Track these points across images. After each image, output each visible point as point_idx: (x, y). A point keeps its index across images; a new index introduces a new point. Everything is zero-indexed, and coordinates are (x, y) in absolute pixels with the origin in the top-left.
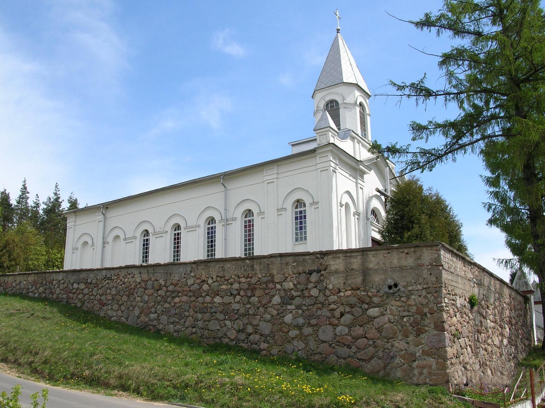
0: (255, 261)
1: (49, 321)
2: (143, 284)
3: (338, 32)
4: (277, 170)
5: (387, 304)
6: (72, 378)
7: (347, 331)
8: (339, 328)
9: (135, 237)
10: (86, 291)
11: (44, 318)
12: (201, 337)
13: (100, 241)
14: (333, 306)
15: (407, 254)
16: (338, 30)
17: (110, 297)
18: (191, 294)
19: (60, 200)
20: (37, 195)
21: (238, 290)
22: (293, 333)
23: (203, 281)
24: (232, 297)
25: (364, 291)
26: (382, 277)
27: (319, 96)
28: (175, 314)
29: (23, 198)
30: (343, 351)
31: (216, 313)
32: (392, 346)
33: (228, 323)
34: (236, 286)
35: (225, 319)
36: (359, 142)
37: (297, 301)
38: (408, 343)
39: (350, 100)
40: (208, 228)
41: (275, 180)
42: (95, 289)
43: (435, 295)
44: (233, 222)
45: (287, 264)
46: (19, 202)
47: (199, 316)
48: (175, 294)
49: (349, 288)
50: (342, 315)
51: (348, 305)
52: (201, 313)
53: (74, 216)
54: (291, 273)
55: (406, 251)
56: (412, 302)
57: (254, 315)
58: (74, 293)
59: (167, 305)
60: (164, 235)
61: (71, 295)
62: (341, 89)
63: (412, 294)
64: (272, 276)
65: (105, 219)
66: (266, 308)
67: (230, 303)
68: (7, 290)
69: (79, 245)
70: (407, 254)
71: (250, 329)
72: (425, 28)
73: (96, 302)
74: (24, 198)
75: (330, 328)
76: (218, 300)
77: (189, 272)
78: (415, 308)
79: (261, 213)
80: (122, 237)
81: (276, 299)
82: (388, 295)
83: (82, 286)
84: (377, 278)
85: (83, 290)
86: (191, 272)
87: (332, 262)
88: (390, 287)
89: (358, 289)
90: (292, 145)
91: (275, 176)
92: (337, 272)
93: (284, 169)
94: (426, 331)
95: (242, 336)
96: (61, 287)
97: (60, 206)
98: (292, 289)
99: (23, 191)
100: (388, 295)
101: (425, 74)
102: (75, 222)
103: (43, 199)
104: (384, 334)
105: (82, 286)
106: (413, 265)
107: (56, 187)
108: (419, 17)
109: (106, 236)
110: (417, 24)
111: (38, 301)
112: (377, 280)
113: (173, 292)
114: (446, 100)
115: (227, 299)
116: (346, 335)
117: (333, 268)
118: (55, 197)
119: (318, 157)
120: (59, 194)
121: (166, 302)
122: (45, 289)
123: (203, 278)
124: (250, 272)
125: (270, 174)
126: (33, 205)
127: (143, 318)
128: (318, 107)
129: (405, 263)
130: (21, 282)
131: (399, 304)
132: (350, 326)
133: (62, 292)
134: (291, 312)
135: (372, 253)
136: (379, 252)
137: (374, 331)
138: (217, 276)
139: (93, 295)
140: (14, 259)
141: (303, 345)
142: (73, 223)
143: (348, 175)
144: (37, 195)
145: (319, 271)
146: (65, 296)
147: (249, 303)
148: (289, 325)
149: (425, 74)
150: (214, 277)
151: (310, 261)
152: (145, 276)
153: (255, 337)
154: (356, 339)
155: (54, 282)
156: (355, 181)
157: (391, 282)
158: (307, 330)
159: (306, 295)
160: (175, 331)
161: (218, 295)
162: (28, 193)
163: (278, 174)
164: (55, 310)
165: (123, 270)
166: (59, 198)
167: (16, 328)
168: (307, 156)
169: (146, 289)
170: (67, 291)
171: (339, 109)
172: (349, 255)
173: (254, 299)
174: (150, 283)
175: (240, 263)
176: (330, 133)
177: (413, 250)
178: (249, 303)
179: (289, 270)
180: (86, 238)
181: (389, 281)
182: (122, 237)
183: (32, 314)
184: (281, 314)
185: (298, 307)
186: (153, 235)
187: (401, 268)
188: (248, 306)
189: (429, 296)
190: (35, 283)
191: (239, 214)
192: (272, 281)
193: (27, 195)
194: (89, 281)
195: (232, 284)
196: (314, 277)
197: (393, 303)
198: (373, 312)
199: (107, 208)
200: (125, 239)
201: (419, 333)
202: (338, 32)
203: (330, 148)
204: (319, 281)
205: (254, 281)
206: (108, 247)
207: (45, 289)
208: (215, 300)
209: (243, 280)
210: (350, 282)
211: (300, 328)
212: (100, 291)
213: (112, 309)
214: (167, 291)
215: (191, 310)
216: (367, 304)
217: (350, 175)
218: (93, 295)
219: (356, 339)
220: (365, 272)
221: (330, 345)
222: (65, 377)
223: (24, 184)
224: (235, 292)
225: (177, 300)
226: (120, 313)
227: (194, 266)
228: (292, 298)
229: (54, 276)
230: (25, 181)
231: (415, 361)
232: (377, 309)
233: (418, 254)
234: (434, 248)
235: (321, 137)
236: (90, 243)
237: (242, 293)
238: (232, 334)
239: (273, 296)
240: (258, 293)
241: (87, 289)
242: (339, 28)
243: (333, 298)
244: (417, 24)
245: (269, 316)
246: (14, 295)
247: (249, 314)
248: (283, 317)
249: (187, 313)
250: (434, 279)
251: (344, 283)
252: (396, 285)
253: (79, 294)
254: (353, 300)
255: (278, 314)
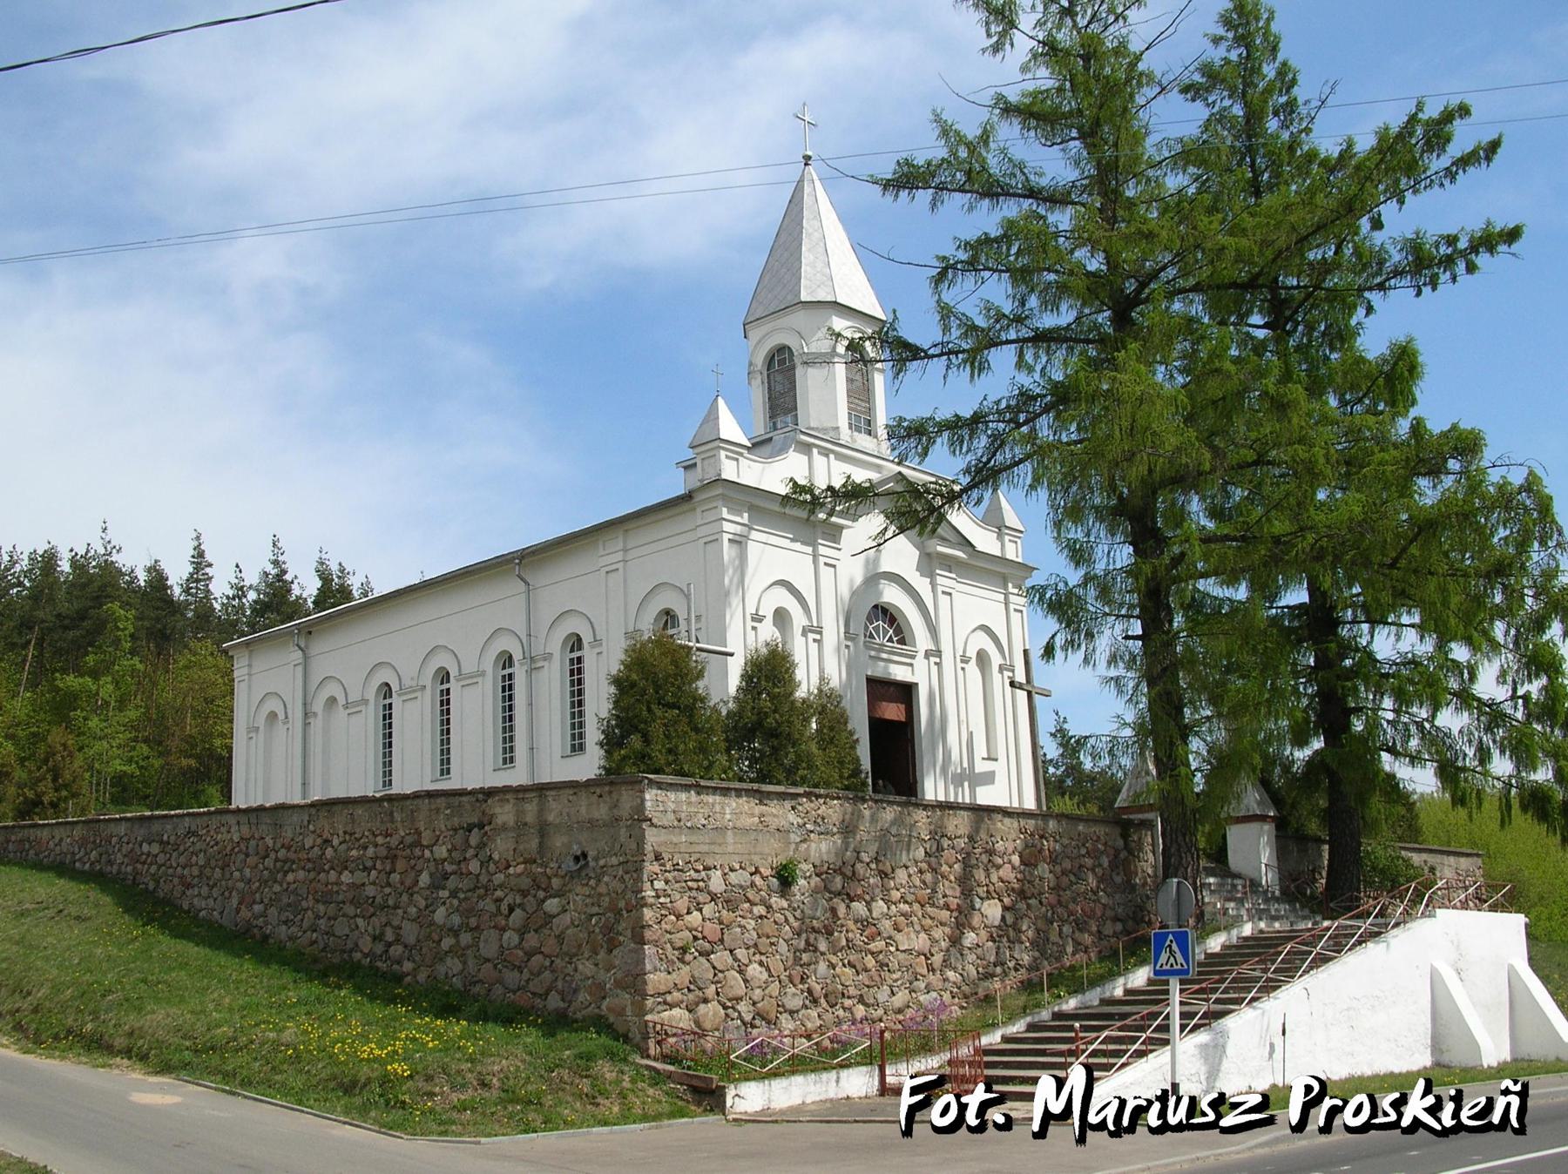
0: (396, 804)
1: (84, 925)
2: (243, 846)
3: (806, 164)
4: (625, 542)
5: (570, 891)
6: (66, 1038)
7: (516, 939)
8: (507, 935)
9: (365, 702)
10: (161, 859)
11: (78, 918)
12: (324, 950)
13: (299, 714)
14: (499, 893)
15: (601, 796)
16: (807, 158)
17: (196, 871)
18: (310, 865)
19: (288, 577)
20: (237, 566)
21: (374, 859)
22: (447, 943)
23: (326, 841)
24: (365, 874)
25: (541, 865)
26: (565, 839)
27: (755, 335)
28: (289, 905)
29: (198, 581)
30: (512, 977)
31: (344, 902)
32: (576, 970)
33: (360, 921)
34: (371, 851)
35: (356, 916)
36: (825, 453)
37: (452, 882)
38: (596, 965)
39: (820, 344)
40: (572, 660)
41: (620, 565)
42: (175, 854)
43: (635, 875)
44: (546, 664)
45: (438, 810)
46: (187, 591)
47: (321, 908)
48: (286, 866)
49: (521, 859)
50: (511, 910)
51: (519, 891)
52: (325, 903)
53: (247, 653)
54: (443, 829)
55: (598, 791)
56: (602, 889)
57: (396, 907)
58: (144, 863)
59: (277, 888)
60: (418, 694)
61: (139, 866)
62: (798, 319)
63: (604, 874)
64: (418, 832)
65: (306, 658)
66: (412, 895)
67: (363, 885)
68: (41, 856)
69: (261, 721)
70: (601, 796)
71: (389, 936)
72: (904, 194)
73: (176, 881)
74: (200, 580)
75: (494, 933)
76: (346, 877)
77: (306, 823)
78: (607, 899)
79: (596, 641)
80: (341, 700)
81: (424, 879)
82: (573, 875)
83: (155, 848)
84: (558, 842)
85: (156, 856)
86: (309, 822)
87: (498, 810)
88: (577, 859)
89: (535, 862)
90: (686, 468)
91: (620, 556)
92: (504, 828)
93: (642, 536)
94: (620, 944)
95: (379, 948)
96: (124, 851)
97: (289, 591)
98: (445, 860)
99: (197, 563)
100: (573, 875)
101: (894, 311)
102: (250, 666)
103: (252, 578)
104: (565, 948)
105: (155, 848)
106: (607, 818)
107: (274, 545)
108: (887, 171)
109: (309, 701)
110: (887, 185)
111: (86, 882)
112: (558, 844)
113: (285, 862)
114: (948, 367)
115: (360, 877)
116: (516, 947)
117: (500, 820)
118: (274, 572)
119: (699, 510)
120: (284, 563)
121: (275, 881)
122: (101, 855)
123: (326, 835)
124: (389, 825)
125: (609, 553)
126: (231, 593)
127: (245, 913)
128: (751, 364)
129: (596, 815)
130: (61, 840)
131: (587, 891)
132: (522, 932)
133: (126, 860)
134: (444, 903)
135: (553, 793)
136: (562, 792)
137: (552, 941)
138: (345, 833)
139: (171, 867)
140: (66, 786)
141: (460, 966)
142: (245, 671)
143: (786, 543)
144: (237, 566)
145: (481, 826)
146: (129, 869)
147: (389, 885)
148: (441, 928)
149: (894, 311)
150: (341, 833)
151: (468, 807)
152: (245, 830)
153: (397, 950)
154: (530, 954)
155: (114, 840)
156: (809, 550)
157: (576, 850)
158: (466, 938)
159: (464, 871)
160: (290, 938)
161: (346, 868)
162: (210, 565)
163: (625, 550)
164: (107, 899)
165: (214, 817)
166: (284, 572)
167: (17, 943)
168: (653, 518)
169: (247, 855)
170: (135, 859)
171: (793, 368)
172: (521, 796)
173: (395, 877)
174: (253, 843)
175: (375, 807)
176: (723, 453)
177: (607, 788)
178: (389, 885)
179: (441, 824)
180: (273, 705)
181: (575, 847)
182: (341, 700)
183: (61, 911)
184: (431, 906)
185: (454, 894)
186: (399, 695)
187: (592, 824)
188: (387, 890)
189: (627, 877)
190: (83, 842)
191: (556, 645)
192: (418, 844)
193: (208, 570)
194: (165, 838)
195: (365, 848)
196: (474, 839)
197: (579, 889)
198: (552, 905)
199: (310, 633)
200: (346, 707)
201: (612, 946)
202: (806, 164)
203: (719, 491)
204: (482, 846)
205: (394, 841)
206: (317, 724)
207: (101, 855)
208: (343, 878)
209: (380, 840)
210: (521, 847)
211: (455, 933)
212: (182, 860)
213: (199, 895)
214: (277, 860)
215: (311, 897)
216: (544, 890)
217: (792, 540)
218: (171, 867)
219: (530, 954)
220: (543, 830)
221: (495, 966)
222: (56, 1037)
223: (196, 543)
224: (369, 864)
225: (290, 877)
226: (211, 901)
227: (313, 811)
228: (446, 876)
229: (112, 828)
230: (198, 538)
231: (604, 998)
232: (556, 900)
233: (615, 796)
234: (637, 787)
235: (706, 462)
236: (281, 716)
237: (379, 866)
238: (366, 944)
239: (421, 871)
240: (401, 865)
241: (162, 855)
242: (809, 153)
243: (499, 878)
244: (887, 185)
245: (415, 910)
246: (39, 866)
247: (388, 907)
248: (434, 912)
249: (304, 904)
250: (634, 846)
251: (515, 850)
252: (585, 855)
253: (151, 864)
254: (525, 882)
255: (427, 907)
